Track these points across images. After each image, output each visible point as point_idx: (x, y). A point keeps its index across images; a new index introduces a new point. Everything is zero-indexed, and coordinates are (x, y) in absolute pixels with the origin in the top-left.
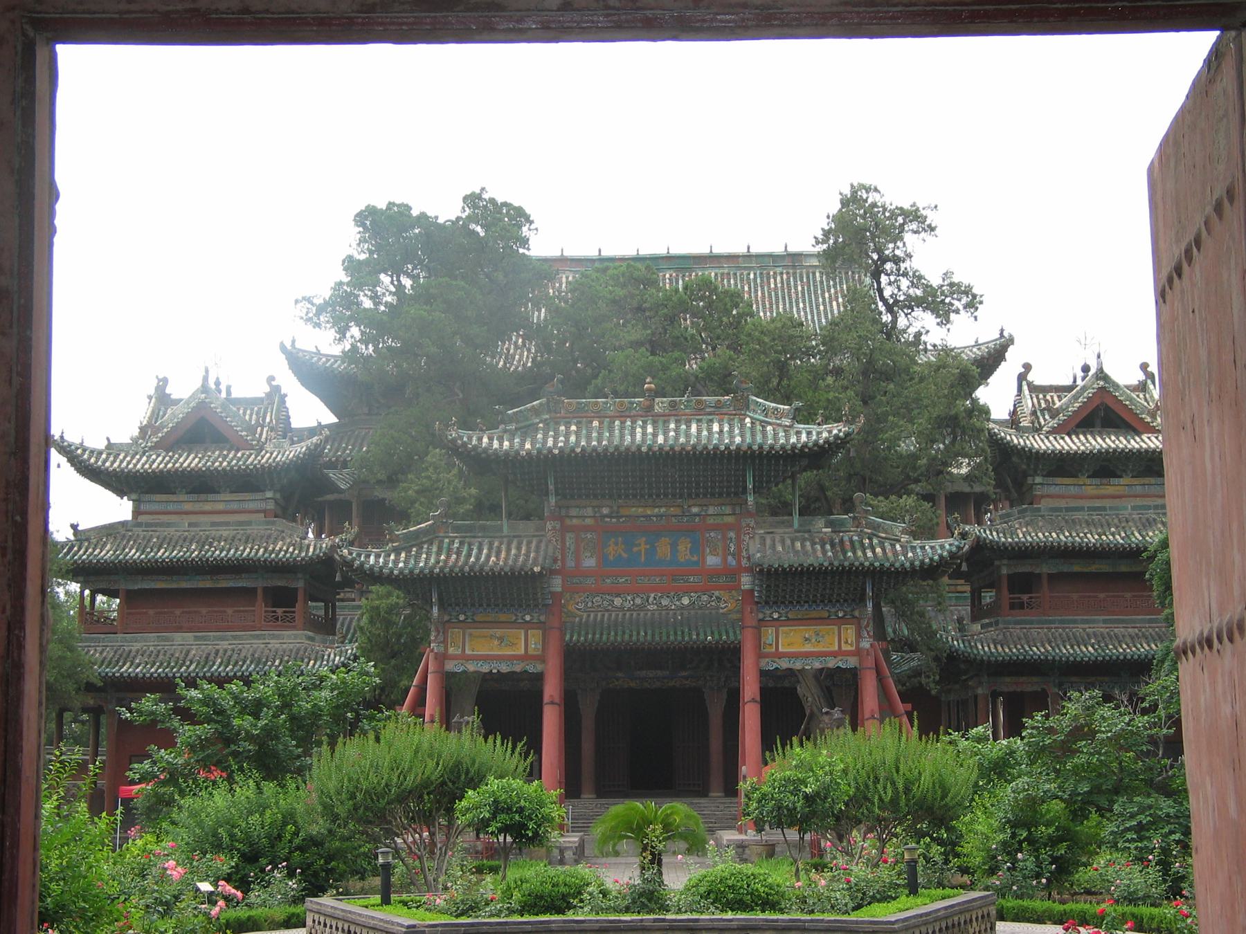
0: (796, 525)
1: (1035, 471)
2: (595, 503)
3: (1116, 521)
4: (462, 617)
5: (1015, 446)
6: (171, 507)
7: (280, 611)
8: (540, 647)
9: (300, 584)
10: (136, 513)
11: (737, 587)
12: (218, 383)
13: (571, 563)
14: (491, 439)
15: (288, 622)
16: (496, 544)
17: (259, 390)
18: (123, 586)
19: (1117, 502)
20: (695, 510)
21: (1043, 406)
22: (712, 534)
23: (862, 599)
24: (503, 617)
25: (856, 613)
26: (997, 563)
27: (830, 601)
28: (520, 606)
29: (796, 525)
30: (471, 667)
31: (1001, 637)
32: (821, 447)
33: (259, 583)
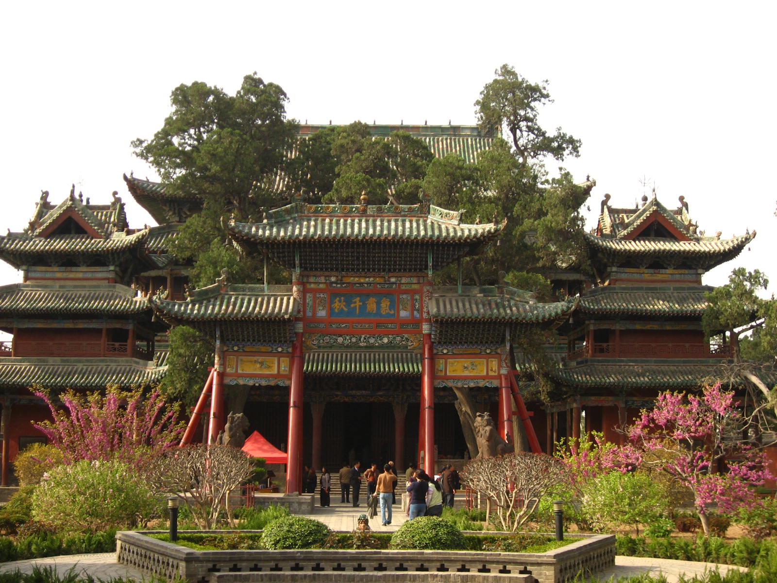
0: (460, 291)
1: (613, 263)
2: (327, 273)
3: (663, 297)
4: (236, 348)
5: (601, 246)
6: (48, 275)
7: (117, 344)
8: (287, 369)
9: (130, 327)
10: (26, 278)
11: (420, 332)
12: (81, 196)
13: (309, 314)
14: (257, 229)
15: (122, 352)
16: (260, 299)
17: (108, 200)
18: (15, 326)
19: (663, 285)
20: (393, 280)
21: (617, 222)
22: (404, 296)
23: (503, 341)
24: (263, 349)
25: (499, 351)
26: (587, 322)
27: (481, 342)
28: (275, 341)
29: (460, 291)
30: (241, 382)
31: (589, 371)
32: (478, 239)
33: (103, 325)
